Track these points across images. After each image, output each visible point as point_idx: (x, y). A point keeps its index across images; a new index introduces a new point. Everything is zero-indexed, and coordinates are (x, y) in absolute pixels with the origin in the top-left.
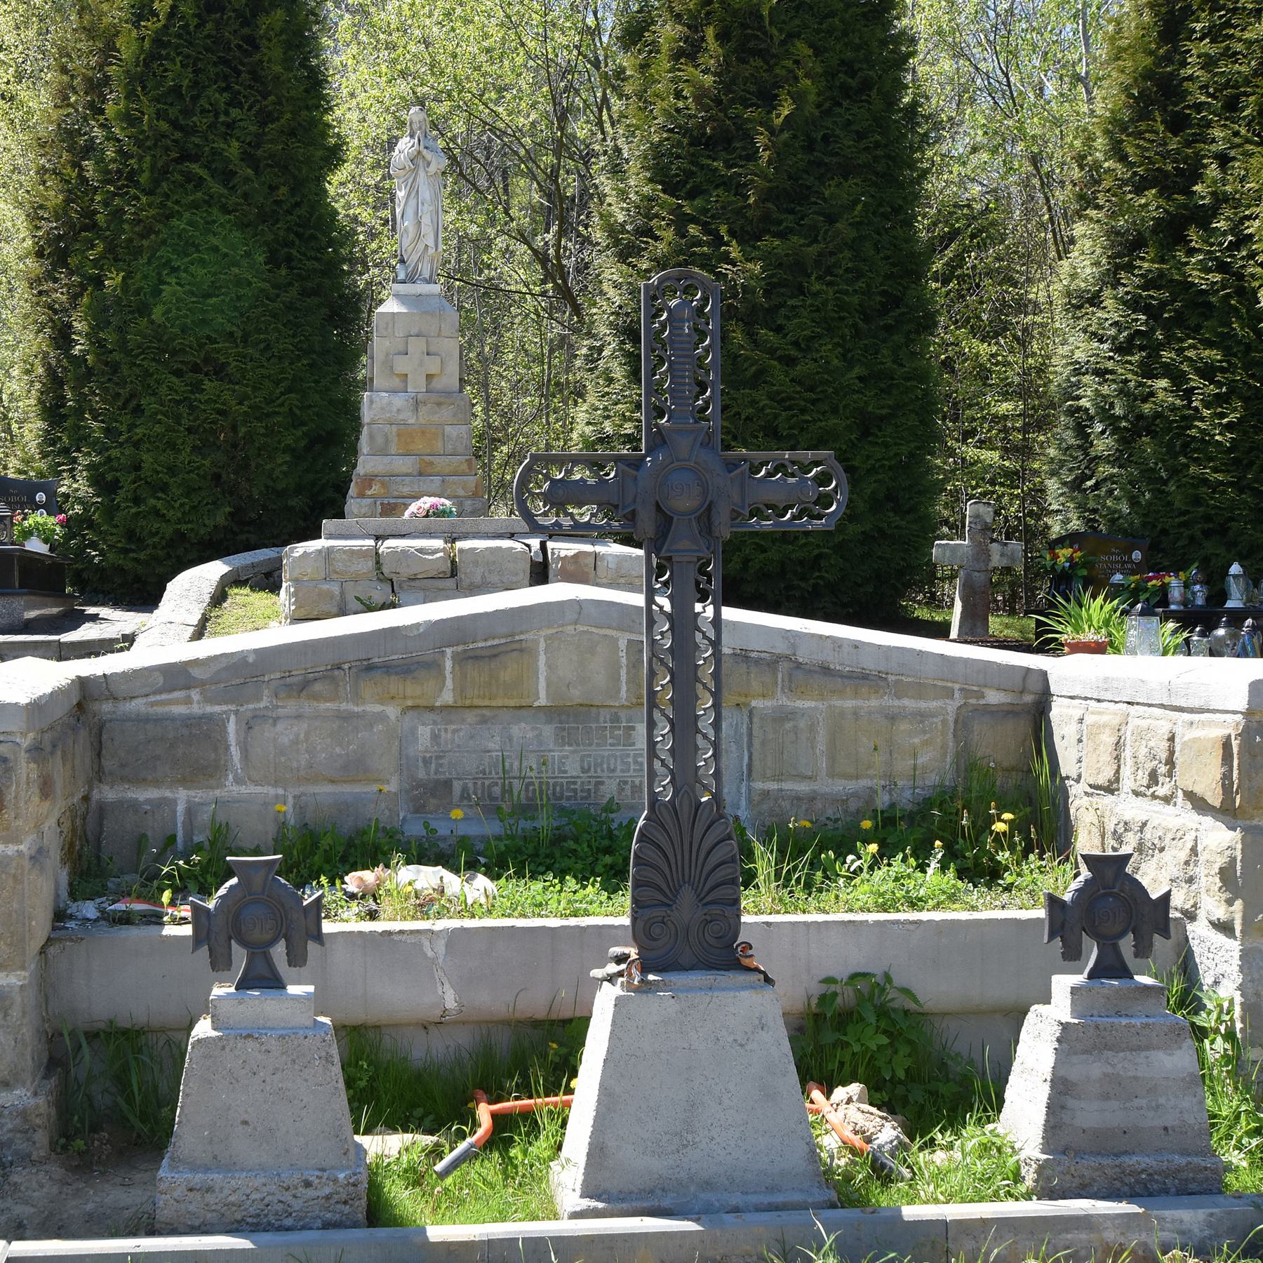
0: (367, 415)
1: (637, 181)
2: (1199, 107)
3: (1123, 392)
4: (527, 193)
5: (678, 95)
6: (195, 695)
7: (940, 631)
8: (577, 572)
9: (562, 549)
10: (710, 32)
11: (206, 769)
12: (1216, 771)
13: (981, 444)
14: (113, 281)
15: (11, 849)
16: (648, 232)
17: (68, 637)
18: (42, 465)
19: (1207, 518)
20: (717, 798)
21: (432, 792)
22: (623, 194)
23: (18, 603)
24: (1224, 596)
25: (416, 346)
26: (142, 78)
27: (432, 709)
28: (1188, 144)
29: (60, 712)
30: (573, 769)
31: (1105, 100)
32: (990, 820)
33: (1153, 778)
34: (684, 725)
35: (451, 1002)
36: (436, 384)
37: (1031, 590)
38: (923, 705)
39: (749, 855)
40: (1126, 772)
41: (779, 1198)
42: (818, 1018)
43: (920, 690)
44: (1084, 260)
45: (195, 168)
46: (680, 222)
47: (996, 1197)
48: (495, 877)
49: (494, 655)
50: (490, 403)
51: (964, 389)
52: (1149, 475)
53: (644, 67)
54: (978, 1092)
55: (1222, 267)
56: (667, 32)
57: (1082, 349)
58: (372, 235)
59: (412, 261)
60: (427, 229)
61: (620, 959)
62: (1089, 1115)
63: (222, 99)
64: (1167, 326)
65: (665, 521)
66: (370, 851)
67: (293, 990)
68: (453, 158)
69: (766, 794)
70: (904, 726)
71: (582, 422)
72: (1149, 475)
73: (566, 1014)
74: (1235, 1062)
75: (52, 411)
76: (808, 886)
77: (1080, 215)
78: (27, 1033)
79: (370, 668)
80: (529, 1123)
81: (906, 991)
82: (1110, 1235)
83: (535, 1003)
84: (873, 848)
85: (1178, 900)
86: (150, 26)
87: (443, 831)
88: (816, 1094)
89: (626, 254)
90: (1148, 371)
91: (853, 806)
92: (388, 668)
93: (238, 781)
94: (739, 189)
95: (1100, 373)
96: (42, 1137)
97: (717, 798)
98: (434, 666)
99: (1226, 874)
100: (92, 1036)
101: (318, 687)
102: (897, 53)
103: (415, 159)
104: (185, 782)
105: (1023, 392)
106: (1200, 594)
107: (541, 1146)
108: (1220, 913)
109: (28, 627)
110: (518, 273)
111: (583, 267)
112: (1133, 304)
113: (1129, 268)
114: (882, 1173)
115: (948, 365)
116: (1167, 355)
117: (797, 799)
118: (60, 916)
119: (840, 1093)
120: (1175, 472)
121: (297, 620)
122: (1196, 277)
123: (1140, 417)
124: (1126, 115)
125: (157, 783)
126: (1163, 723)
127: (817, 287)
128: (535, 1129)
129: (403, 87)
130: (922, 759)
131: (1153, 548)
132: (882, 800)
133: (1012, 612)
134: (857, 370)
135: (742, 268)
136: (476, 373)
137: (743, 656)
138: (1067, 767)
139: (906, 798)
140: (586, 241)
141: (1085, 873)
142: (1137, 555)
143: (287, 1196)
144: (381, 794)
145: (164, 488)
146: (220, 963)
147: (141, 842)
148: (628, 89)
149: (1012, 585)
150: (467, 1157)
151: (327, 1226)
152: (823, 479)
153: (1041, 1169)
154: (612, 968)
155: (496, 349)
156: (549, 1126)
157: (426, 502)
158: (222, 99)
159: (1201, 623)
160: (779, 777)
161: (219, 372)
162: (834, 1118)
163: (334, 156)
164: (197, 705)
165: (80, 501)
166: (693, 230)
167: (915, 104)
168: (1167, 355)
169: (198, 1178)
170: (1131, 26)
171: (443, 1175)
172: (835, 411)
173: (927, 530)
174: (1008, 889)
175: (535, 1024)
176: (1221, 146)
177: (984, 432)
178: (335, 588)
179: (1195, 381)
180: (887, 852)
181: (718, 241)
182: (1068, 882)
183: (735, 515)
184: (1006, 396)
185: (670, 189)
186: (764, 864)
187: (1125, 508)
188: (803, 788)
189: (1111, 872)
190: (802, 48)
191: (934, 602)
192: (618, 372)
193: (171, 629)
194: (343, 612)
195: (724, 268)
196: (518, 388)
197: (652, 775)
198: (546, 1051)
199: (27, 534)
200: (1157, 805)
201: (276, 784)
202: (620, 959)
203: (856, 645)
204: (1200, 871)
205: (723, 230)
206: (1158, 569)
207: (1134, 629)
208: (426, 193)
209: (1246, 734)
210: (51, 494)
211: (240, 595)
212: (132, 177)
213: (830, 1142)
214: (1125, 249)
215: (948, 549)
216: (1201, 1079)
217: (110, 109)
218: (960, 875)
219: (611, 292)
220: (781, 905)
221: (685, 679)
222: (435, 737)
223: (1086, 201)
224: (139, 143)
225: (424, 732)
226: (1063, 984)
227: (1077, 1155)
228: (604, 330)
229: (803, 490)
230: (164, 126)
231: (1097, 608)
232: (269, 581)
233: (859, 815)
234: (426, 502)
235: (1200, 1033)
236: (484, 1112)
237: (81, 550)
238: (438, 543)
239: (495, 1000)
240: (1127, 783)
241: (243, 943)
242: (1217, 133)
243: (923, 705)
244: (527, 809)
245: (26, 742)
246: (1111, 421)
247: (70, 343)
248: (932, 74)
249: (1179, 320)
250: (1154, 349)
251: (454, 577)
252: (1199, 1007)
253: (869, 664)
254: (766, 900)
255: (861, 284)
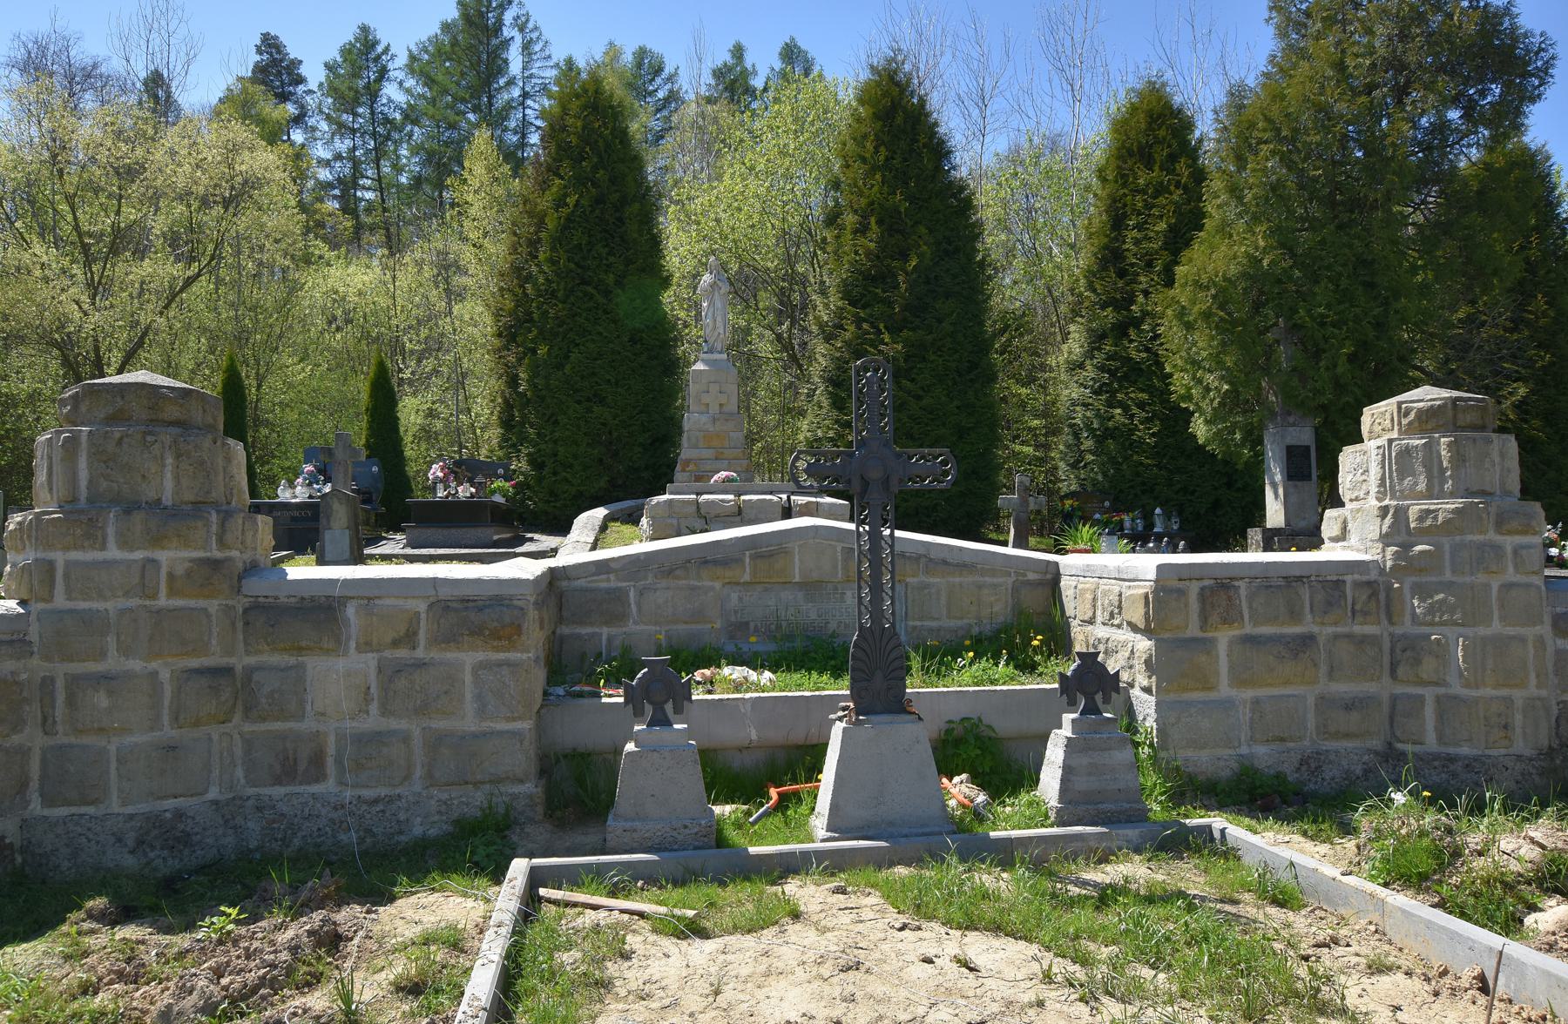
0: (686, 426)
1: (835, 300)
2: (1132, 265)
3: (1098, 416)
4: (767, 299)
5: (856, 253)
6: (612, 577)
7: (1005, 544)
8: (808, 510)
9: (801, 500)
10: (873, 220)
11: (618, 618)
12: (1142, 611)
13: (1023, 443)
14: (542, 351)
15: (525, 656)
16: (841, 327)
17: (518, 550)
18: (500, 453)
19: (1144, 484)
20: (893, 625)
21: (739, 628)
22: (827, 306)
23: (489, 531)
24: (1152, 525)
25: (714, 388)
26: (557, 242)
27: (738, 584)
28: (1128, 284)
29: (544, 585)
30: (813, 616)
31: (1083, 261)
32: (1031, 639)
33: (1112, 616)
34: (876, 589)
35: (754, 736)
36: (725, 409)
37: (1052, 524)
38: (995, 580)
39: (908, 659)
40: (1099, 613)
41: (927, 830)
42: (945, 742)
43: (993, 572)
44: (1075, 344)
45: (589, 289)
46: (858, 322)
47: (1036, 826)
48: (774, 672)
49: (771, 555)
50: (751, 418)
51: (1013, 413)
52: (1113, 461)
53: (838, 237)
54: (1027, 777)
55: (1147, 350)
56: (850, 219)
57: (1076, 393)
58: (686, 325)
59: (711, 341)
60: (719, 324)
61: (844, 709)
62: (1081, 784)
63: (604, 251)
64: (1120, 380)
65: (866, 484)
66: (711, 658)
67: (676, 726)
68: (732, 284)
69: (915, 628)
70: (986, 591)
71: (805, 429)
72: (1113, 461)
73: (815, 742)
74: (1154, 758)
75: (507, 423)
76: (938, 674)
77: (1073, 321)
78: (532, 753)
79: (706, 562)
80: (797, 797)
81: (990, 727)
82: (1093, 844)
83: (798, 737)
84: (971, 654)
85: (1125, 676)
86: (565, 211)
87: (745, 649)
88: (945, 780)
89: (828, 338)
90: (1110, 404)
91: (960, 633)
92: (715, 562)
93: (635, 623)
94: (890, 304)
95: (1085, 405)
96: (540, 809)
97: (893, 625)
98: (739, 561)
99: (1147, 662)
100: (565, 756)
101: (678, 572)
102: (974, 232)
103: (713, 285)
104: (607, 623)
105: (1044, 415)
106: (1140, 524)
107: (804, 809)
108: (1145, 683)
109: (495, 545)
110: (764, 346)
111: (804, 345)
112: (1102, 368)
113: (1099, 349)
114: (978, 816)
115: (1004, 399)
116: (1120, 396)
117: (931, 630)
118: (545, 693)
119: (956, 779)
120: (1126, 458)
121: (653, 539)
122: (1134, 354)
123: (1107, 429)
124: (1095, 268)
125: (592, 624)
126: (1116, 587)
127: (933, 358)
128: (800, 801)
129: (705, 245)
130: (996, 608)
131: (1116, 500)
132: (975, 631)
133: (1042, 535)
134: (956, 403)
135: (892, 347)
136: (745, 405)
137: (902, 555)
138: (1069, 612)
139: (987, 629)
140: (804, 330)
141: (1078, 662)
142: (1107, 504)
143: (675, 834)
144: (712, 629)
145: (571, 466)
146: (638, 714)
147: (583, 656)
148: (829, 249)
149: (1042, 521)
150: (766, 814)
151: (696, 848)
152: (944, 463)
153: (1059, 811)
154: (840, 713)
155: (754, 389)
156: (807, 800)
157: (723, 474)
158: (604, 251)
159: (1140, 540)
160: (921, 619)
161: (602, 401)
162: (954, 791)
163: (666, 282)
164: (614, 582)
165: (522, 473)
166: (865, 326)
167: (984, 258)
168: (1120, 396)
169: (628, 825)
170: (1096, 221)
171: (753, 824)
172: (944, 424)
173: (995, 490)
174: (1040, 675)
175: (798, 747)
176: (1144, 286)
177: (1025, 436)
178: (675, 522)
179: (1135, 410)
180: (978, 656)
181: (879, 332)
182: (1070, 668)
183: (901, 481)
184: (1036, 417)
185: (853, 303)
186: (915, 663)
187: (1100, 478)
188: (934, 624)
189: (1089, 659)
190: (922, 230)
191: (999, 530)
192: (825, 403)
193: (579, 545)
194: (679, 535)
195: (882, 347)
196: (766, 411)
197: (860, 613)
198: (808, 760)
199: (493, 492)
200: (1114, 630)
201: (656, 624)
202: (844, 709)
203: (961, 549)
204: (1136, 662)
205: (881, 326)
206: (1118, 511)
207: (1104, 542)
208: (718, 304)
209: (1156, 591)
210: (506, 468)
211: (615, 526)
212: (553, 294)
213: (952, 803)
214: (1096, 339)
215: (1007, 500)
216: (1136, 765)
217: (542, 257)
218: (1016, 667)
219: (821, 359)
220: (925, 684)
221: (876, 565)
222: (740, 599)
223: (1075, 313)
224: (557, 275)
225: (734, 596)
226: (1068, 718)
227: (1075, 805)
228: (817, 380)
229: (935, 469)
230: (572, 266)
231: (1086, 531)
232: (632, 518)
233: (964, 638)
234: (723, 474)
235: (1137, 745)
236: (773, 792)
237: (523, 501)
238: (731, 497)
239: (777, 735)
240: (1099, 619)
241: (650, 702)
242: (1142, 279)
243: (995, 580)
244: (790, 637)
245: (532, 600)
246: (1092, 431)
247: (518, 385)
248: (992, 241)
249: (1126, 377)
250: (1113, 393)
251: (739, 516)
252: (1136, 732)
253: (967, 559)
254: (917, 681)
255: (956, 356)
